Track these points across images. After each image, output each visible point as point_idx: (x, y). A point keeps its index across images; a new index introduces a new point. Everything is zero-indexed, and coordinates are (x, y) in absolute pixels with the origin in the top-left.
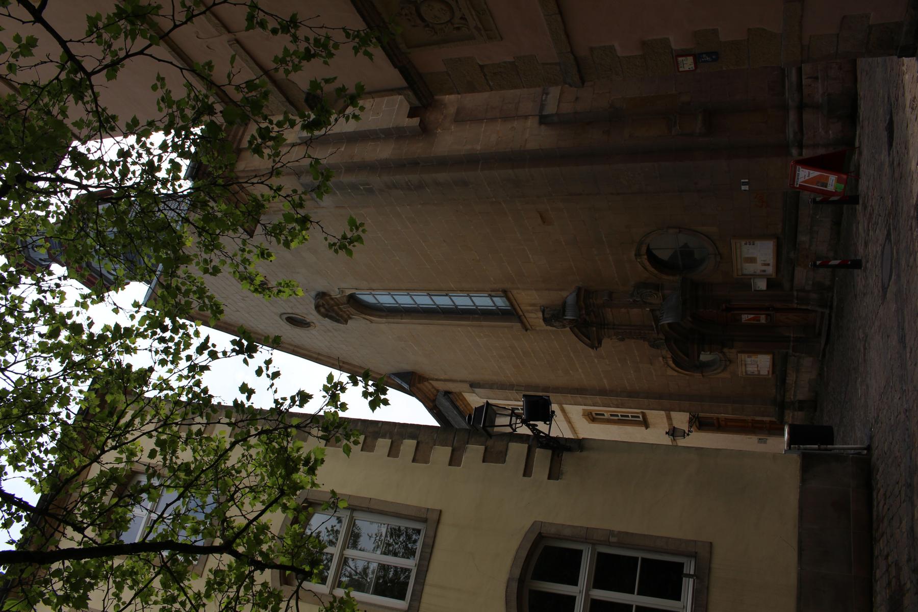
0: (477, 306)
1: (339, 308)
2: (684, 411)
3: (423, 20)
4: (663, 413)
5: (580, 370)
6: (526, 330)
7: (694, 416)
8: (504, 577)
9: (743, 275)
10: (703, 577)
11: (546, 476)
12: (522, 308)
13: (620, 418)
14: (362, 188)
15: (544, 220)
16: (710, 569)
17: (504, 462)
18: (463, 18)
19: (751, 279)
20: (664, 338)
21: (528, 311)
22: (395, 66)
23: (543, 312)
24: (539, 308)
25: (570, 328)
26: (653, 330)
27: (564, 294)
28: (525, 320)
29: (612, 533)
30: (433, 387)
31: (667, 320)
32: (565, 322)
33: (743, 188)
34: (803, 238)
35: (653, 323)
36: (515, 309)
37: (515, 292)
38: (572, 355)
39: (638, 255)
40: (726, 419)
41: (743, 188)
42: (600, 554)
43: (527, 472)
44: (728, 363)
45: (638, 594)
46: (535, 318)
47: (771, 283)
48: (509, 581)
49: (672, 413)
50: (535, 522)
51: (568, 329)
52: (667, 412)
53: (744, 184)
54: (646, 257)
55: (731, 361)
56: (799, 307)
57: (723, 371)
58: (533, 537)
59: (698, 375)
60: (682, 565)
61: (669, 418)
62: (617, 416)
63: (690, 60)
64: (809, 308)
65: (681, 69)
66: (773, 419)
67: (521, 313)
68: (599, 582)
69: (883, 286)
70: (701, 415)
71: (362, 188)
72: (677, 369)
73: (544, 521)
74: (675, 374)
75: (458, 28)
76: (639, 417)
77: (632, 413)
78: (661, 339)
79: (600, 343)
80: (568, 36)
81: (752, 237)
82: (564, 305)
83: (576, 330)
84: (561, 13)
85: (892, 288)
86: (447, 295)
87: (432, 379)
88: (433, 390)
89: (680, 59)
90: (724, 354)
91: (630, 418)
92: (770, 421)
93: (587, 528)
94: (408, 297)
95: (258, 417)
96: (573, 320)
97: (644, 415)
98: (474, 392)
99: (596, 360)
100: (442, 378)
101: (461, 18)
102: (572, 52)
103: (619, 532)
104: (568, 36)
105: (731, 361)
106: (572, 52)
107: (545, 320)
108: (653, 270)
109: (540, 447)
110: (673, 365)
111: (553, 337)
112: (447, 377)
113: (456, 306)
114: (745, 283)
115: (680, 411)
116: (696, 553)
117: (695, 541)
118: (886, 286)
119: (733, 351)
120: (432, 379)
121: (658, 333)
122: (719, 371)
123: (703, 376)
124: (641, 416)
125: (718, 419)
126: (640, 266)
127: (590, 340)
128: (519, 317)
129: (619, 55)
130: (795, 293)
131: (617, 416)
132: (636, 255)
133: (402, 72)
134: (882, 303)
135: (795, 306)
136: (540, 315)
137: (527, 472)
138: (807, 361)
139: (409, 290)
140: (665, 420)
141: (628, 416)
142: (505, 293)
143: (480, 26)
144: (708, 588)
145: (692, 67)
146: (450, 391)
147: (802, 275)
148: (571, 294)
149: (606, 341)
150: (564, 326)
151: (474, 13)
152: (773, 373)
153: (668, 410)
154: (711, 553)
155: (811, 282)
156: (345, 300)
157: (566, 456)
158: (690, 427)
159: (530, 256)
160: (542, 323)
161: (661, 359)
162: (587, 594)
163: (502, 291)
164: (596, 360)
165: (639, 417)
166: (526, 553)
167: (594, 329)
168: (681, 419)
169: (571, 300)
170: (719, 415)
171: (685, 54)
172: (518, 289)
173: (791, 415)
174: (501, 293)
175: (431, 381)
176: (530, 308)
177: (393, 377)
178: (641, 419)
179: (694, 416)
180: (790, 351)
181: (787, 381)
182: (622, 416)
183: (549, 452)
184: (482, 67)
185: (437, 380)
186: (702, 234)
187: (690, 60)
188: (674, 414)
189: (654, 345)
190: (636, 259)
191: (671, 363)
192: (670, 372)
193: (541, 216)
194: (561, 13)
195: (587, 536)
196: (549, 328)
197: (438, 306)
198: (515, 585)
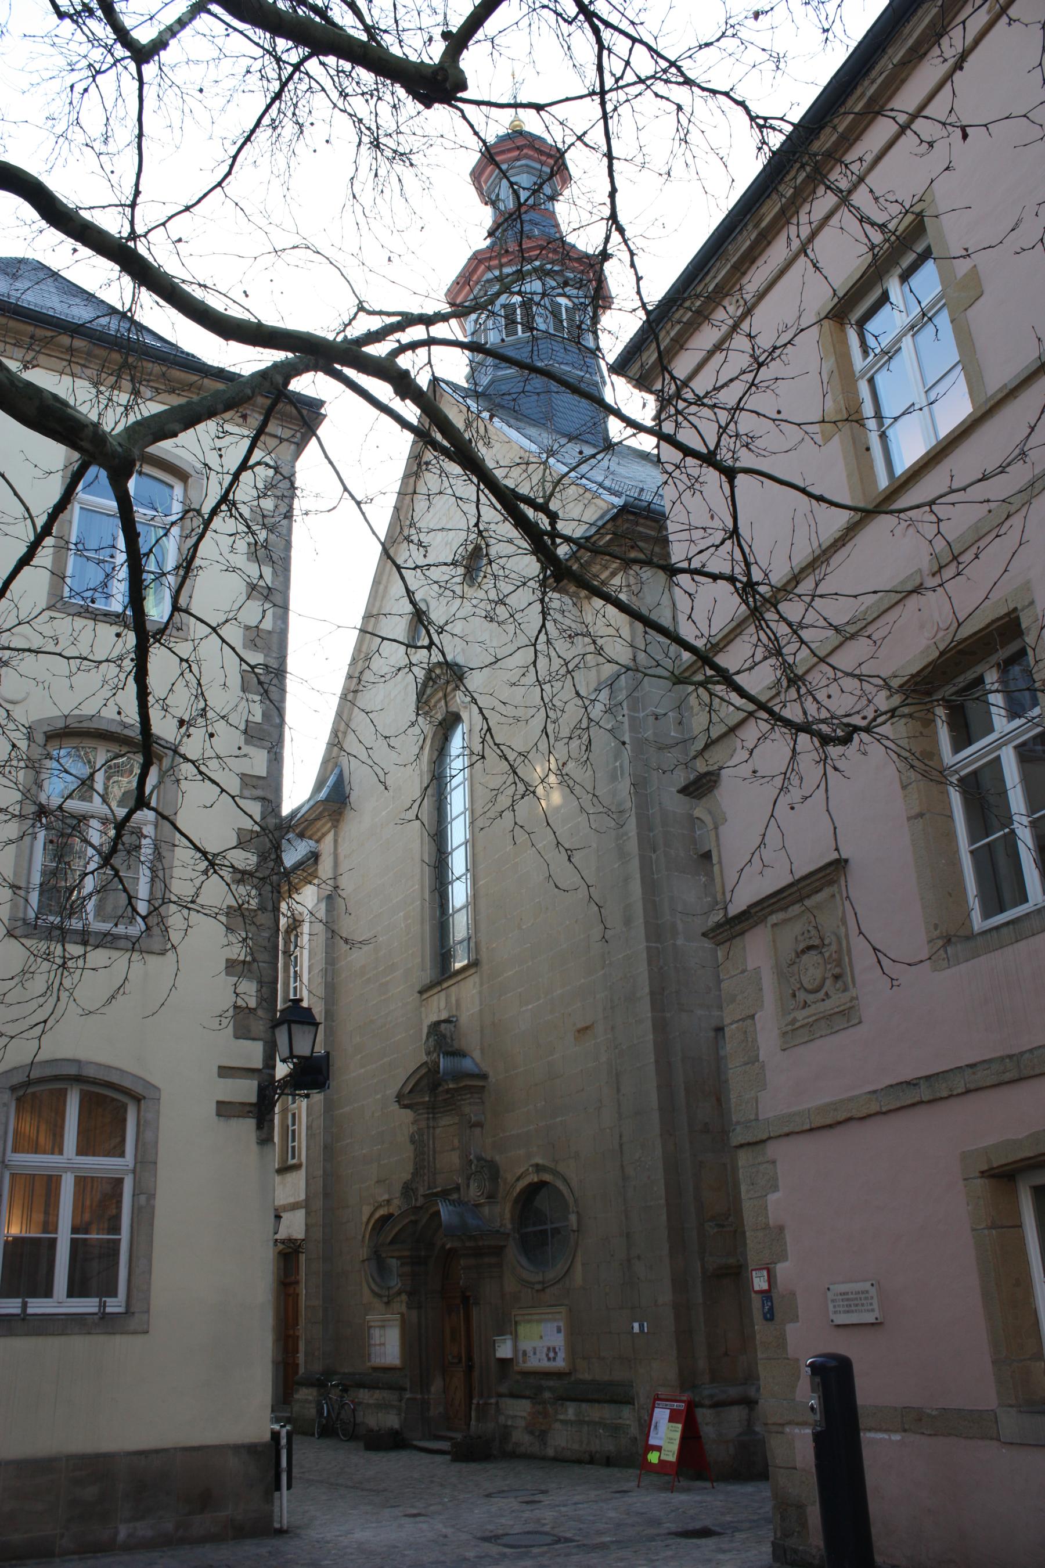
0: (451, 823)
1: (439, 700)
2: (307, 1231)
3: (803, 952)
4: (303, 1197)
5: (363, 1070)
6: (421, 992)
7: (299, 1246)
8: (82, 1055)
9: (516, 1323)
10: (105, 1323)
11: (221, 1099)
12: (453, 988)
13: (291, 1128)
14: (618, 764)
15: (583, 1031)
16: (114, 1334)
17: (237, 1037)
18: (805, 1005)
19: (511, 1334)
20: (418, 1204)
21: (448, 997)
22: (750, 907)
23: (447, 1021)
24: (454, 1013)
25: (426, 1063)
26: (429, 1188)
27: (477, 1055)
28: (435, 990)
29: (152, 1196)
30: (324, 835)
31: (445, 1211)
32: (435, 1055)
33: (636, 1326)
34: (571, 1411)
35: (439, 1189)
36: (450, 977)
37: (476, 978)
38: (385, 1060)
39: (539, 1168)
40: (298, 1295)
41: (636, 1326)
42: (119, 1182)
43: (225, 1072)
44: (385, 1299)
45: (72, 1239)
46: (437, 1009)
47: (504, 1363)
48: (78, 1062)
49: (303, 1211)
50: (158, 1089)
51: (425, 1058)
52: (304, 1204)
53: (641, 1326)
54: (536, 1180)
55: (388, 1303)
56: (474, 1407)
57: (372, 1291)
58: (139, 1089)
59: (364, 1253)
60: (114, 1294)
61: (294, 1207)
62: (294, 1124)
63: (765, 1286)
64: (473, 1423)
65: (754, 1273)
66: (302, 1370)
67: (445, 985)
68: (82, 1183)
69: (497, 1537)
70: (303, 1258)
71: (618, 764)
72: (372, 1221)
73: (162, 1101)
74: (365, 1219)
75: (794, 995)
76: (293, 1157)
77: (300, 1148)
78: (416, 1200)
79: (406, 1107)
80: (787, 1135)
81: (574, 1332)
82: (459, 1054)
83: (424, 1071)
84: (811, 1130)
85: (494, 1549)
86: (467, 870)
87: (336, 835)
88: (319, 834)
89: (765, 1273)
90: (399, 1293)
91: (290, 1145)
92: (298, 1365)
93: (156, 1163)
94: (462, 809)
95: (316, 881)
96: (439, 1067)
97: (297, 1167)
98: (319, 901)
99: (379, 1096)
100: (340, 850)
101: (805, 1002)
102: (770, 1138)
103: (153, 1207)
104: (787, 1135)
105: (388, 1303)
106: (770, 1138)
107: (437, 1024)
108: (518, 1189)
109: (259, 1085)
110: (377, 1215)
111: (411, 1032)
112: (341, 857)
113: (451, 883)
114: (505, 1325)
115: (306, 1225)
116: (133, 1313)
117: (148, 1311)
118: (499, 1541)
119: (404, 1309)
120: (336, 835)
121: (424, 1196)
122: (373, 1286)
123: (363, 1261)
124: (295, 1161)
125: (297, 1283)
126: (522, 1170)
127: (410, 1092)
128: (439, 983)
129: (769, 1196)
130: (493, 1401)
131: (294, 1124)
132: (537, 1165)
133: (743, 913)
134: (475, 1537)
135: (475, 1401)
136: (444, 1016)
137: (225, 1072)
138: (254, 859)
139: (472, 843)
140: (292, 1200)
141: (293, 1141)
142: (474, 964)
143: (798, 1024)
144: (89, 1333)
145: (756, 1288)
146: (320, 862)
147: (519, 1410)
148: (477, 1065)
149: (408, 1115)
150: (428, 1053)
151: (810, 1020)
152: (375, 1369)
153: (306, 1205)
154: (135, 1333)
155: (509, 1423)
156: (453, 709)
157: (251, 1123)
158: (283, 1242)
159: (530, 1007)
160: (434, 1018)
161: (386, 1197)
162: (66, 1170)
163: (477, 959)
164: (379, 1096)
165: (293, 1157)
166: (115, 1081)
167: (427, 1099)
168: (294, 1226)
169: (467, 1064)
170: (303, 1285)
171: (771, 1279)
172: (481, 984)
173: (310, 1398)
174: (473, 956)
175: (332, 832)
176: (453, 1000)
177: (336, 771)
178: (291, 1162)
179: (299, 1246)
180: (408, 1395)
181: (362, 1390)
182: (294, 1131)
183: (253, 1099)
184: (752, 1017)
185: (336, 841)
186: (572, 1262)
187: (765, 1286)
188: (301, 1214)
189: (408, 1190)
190: (532, 1166)
191: (381, 1212)
192: (367, 1210)
193: (587, 1028)
194: (811, 1130)
195: (146, 1162)
196: (425, 1031)
197: (451, 853)
198: (73, 1071)
